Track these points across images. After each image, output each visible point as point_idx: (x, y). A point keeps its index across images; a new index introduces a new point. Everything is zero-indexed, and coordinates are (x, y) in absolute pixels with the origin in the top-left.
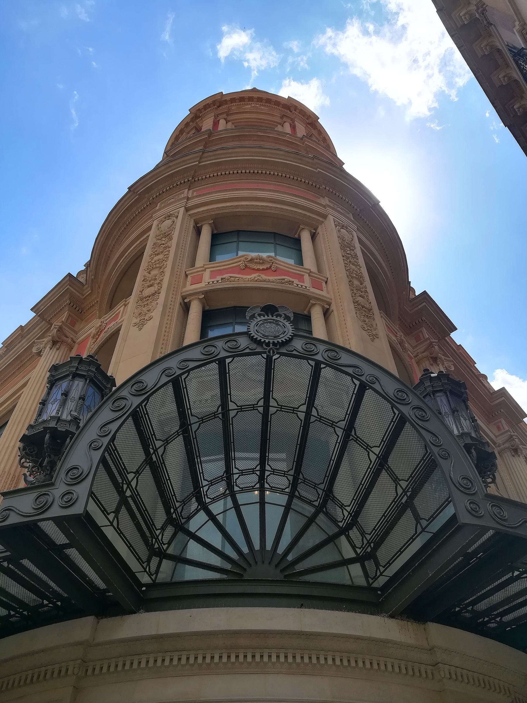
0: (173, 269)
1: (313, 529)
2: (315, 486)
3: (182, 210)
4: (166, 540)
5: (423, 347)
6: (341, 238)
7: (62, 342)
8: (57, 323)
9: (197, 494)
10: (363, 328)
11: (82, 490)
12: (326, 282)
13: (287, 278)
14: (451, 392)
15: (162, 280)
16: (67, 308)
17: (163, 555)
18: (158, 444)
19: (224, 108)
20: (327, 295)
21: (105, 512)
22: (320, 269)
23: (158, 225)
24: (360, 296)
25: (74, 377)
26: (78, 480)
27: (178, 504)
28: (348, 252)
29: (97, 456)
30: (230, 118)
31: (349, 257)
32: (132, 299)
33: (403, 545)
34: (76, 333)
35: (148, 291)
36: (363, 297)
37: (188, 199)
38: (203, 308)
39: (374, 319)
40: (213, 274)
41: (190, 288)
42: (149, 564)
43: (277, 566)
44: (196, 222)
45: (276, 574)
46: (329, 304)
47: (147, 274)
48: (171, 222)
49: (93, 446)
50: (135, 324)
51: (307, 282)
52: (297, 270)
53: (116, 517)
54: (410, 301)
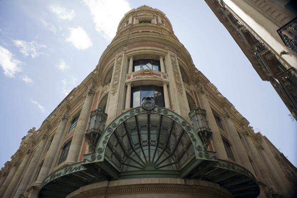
0: (122, 75)
1: (163, 155)
2: (163, 145)
3: (124, 54)
4: (124, 160)
5: (199, 88)
6: (172, 60)
7: (92, 93)
8: (89, 88)
9: (132, 147)
10: (178, 91)
11: (103, 154)
12: (168, 76)
13: (156, 76)
14: (201, 113)
15: (119, 79)
16: (92, 83)
17: (124, 164)
18: (120, 138)
19: (135, 15)
20: (168, 81)
21: (108, 158)
22: (166, 72)
23: (117, 59)
24: (178, 80)
25: (97, 115)
26: (101, 152)
27: (127, 151)
28: (174, 65)
29: (106, 145)
30: (137, 18)
31: (174, 67)
32: (111, 84)
33: (185, 161)
34: (95, 90)
35: (115, 82)
36: (179, 80)
37: (125, 50)
38: (131, 86)
39: (182, 87)
40: (134, 76)
41: (127, 81)
42: (121, 168)
43: (153, 166)
44: (128, 58)
45: (152, 168)
46: (169, 83)
47: (115, 77)
48: (120, 61)
49: (104, 142)
50: (112, 94)
51: (162, 77)
52: (159, 73)
53: (111, 158)
54: (195, 74)
